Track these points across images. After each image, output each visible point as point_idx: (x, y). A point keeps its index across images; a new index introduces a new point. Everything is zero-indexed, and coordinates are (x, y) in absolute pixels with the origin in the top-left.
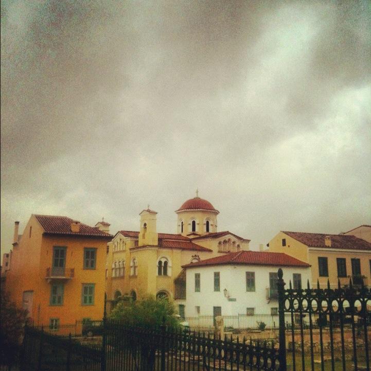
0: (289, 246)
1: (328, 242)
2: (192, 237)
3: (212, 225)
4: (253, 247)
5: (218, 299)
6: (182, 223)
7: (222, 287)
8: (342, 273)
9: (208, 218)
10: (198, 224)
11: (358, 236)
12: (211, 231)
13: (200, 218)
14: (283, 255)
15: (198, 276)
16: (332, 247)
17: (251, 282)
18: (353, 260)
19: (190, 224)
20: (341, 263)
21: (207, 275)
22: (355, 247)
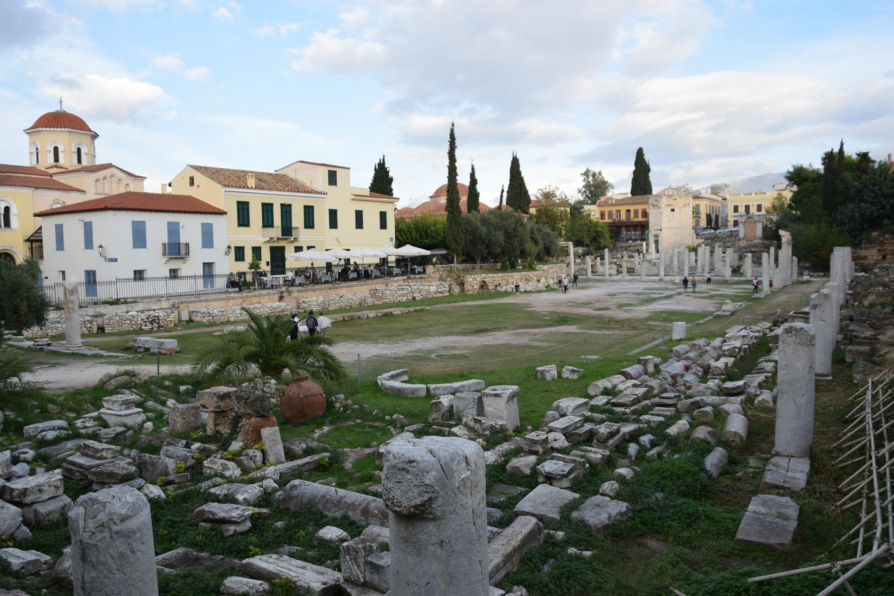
0: (198, 186)
1: (251, 182)
2: (55, 170)
3: (86, 154)
4: (152, 186)
5: (91, 260)
6: (37, 149)
7: (96, 244)
8: (267, 222)
9: (78, 144)
10: (64, 152)
11: (292, 175)
12: (85, 162)
13: (64, 139)
14: (189, 199)
15: (59, 229)
16: (256, 188)
17: (139, 238)
18: (282, 205)
19: (50, 151)
20: (267, 209)
21: (73, 225)
22: (287, 189)
